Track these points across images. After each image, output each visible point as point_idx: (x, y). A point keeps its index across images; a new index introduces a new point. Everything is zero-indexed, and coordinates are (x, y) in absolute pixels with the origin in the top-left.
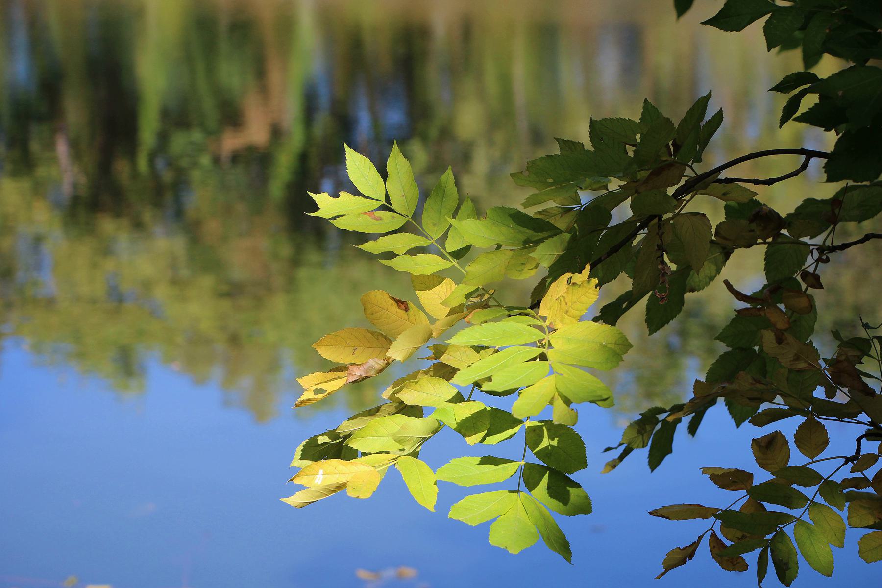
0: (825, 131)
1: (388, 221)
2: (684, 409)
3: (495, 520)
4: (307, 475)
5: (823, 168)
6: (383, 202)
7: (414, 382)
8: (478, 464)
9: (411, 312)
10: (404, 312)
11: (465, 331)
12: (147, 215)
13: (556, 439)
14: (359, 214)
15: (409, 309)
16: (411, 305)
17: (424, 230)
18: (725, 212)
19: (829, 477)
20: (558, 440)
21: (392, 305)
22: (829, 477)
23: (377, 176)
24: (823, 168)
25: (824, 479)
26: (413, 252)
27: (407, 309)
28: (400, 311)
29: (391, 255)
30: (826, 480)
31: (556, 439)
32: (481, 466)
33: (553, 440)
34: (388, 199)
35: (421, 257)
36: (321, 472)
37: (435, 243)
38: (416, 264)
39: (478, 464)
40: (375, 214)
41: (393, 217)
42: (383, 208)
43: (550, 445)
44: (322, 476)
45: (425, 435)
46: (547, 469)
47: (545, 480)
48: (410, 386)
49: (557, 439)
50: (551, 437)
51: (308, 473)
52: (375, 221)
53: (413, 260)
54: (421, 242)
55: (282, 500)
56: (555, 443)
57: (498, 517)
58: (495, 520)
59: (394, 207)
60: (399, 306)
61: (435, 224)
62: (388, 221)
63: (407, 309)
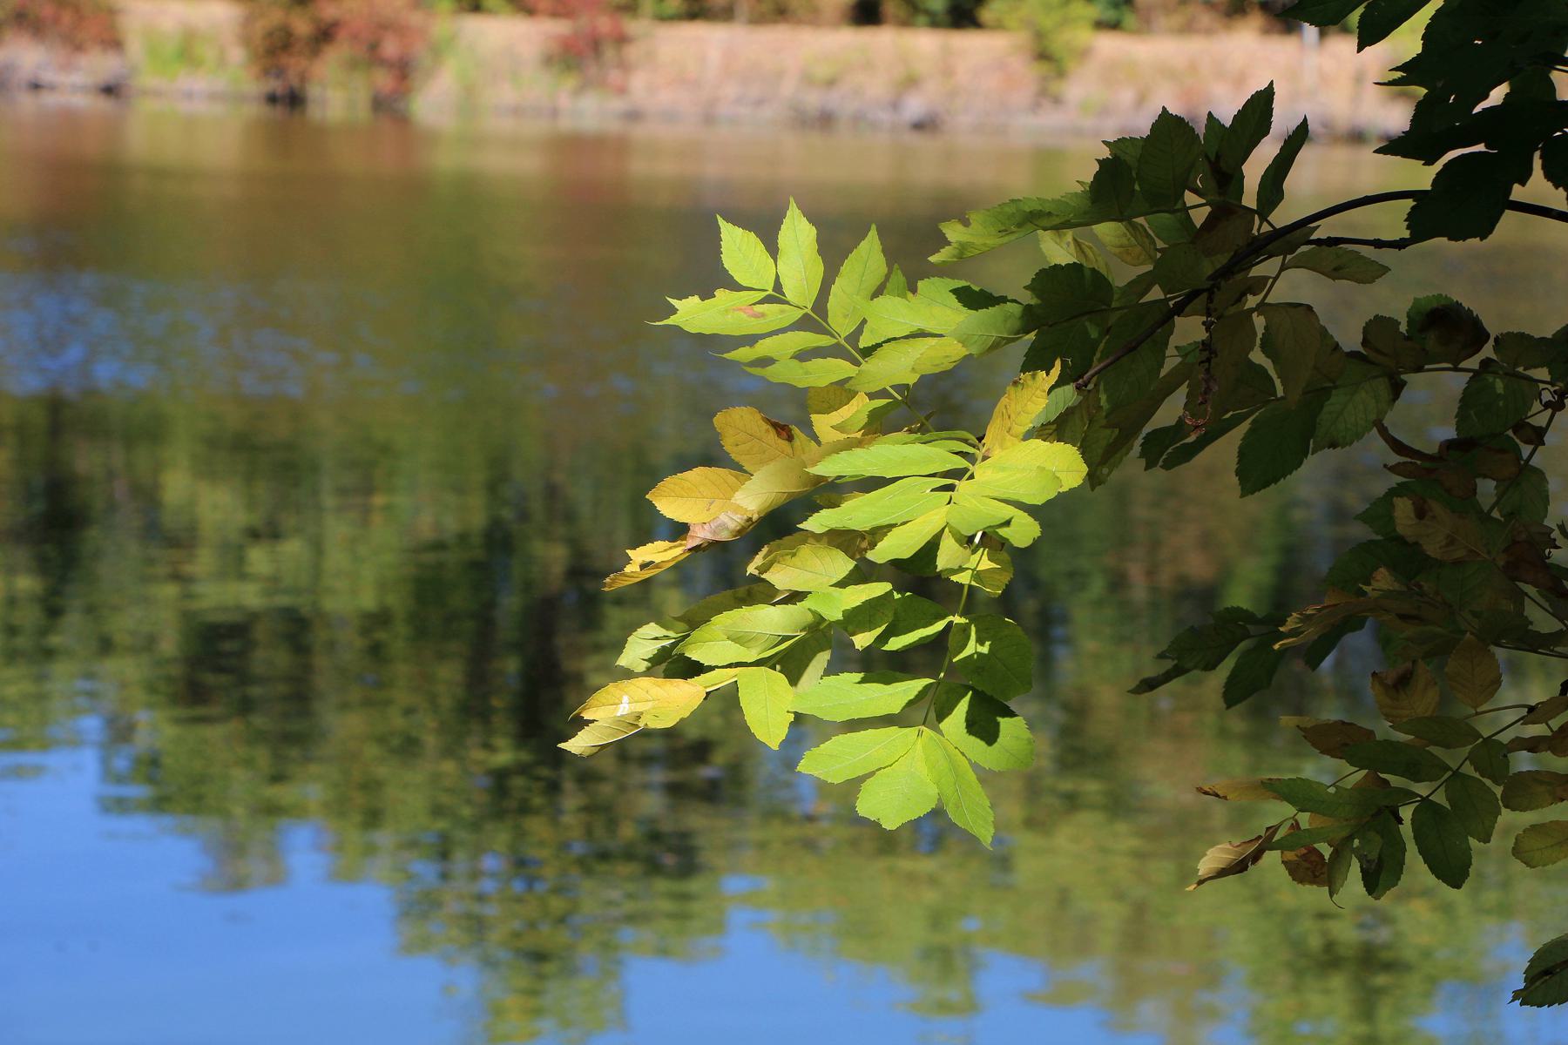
0: (1423, 164)
1: (775, 315)
2: (1287, 623)
3: (872, 774)
4: (604, 705)
5: (1406, 220)
6: (770, 292)
7: (790, 553)
8: (859, 683)
9: (797, 442)
10: (786, 443)
11: (839, 455)
12: (1296, 859)
13: (988, 643)
14: (726, 311)
15: (793, 438)
16: (796, 431)
17: (829, 325)
18: (957, 298)
19: (1494, 735)
20: (990, 645)
21: (767, 431)
22: (1494, 735)
23: (765, 257)
24: (1406, 220)
25: (1482, 737)
26: (803, 356)
27: (790, 438)
28: (780, 441)
29: (766, 362)
30: (1488, 741)
31: (988, 643)
32: (864, 685)
33: (982, 644)
34: (778, 286)
35: (818, 363)
36: (625, 699)
37: (843, 342)
38: (806, 373)
39: (859, 683)
40: (755, 309)
41: (782, 312)
42: (768, 300)
43: (976, 652)
44: (627, 706)
45: (786, 632)
46: (971, 688)
47: (963, 707)
48: (784, 560)
49: (1327, 857)
50: (980, 641)
51: (604, 701)
52: (753, 319)
53: (803, 368)
54: (824, 341)
55: (559, 745)
56: (985, 649)
57: (880, 769)
58: (872, 774)
59: (789, 296)
60: (779, 434)
61: (848, 315)
62: (775, 315)
63: (790, 438)
